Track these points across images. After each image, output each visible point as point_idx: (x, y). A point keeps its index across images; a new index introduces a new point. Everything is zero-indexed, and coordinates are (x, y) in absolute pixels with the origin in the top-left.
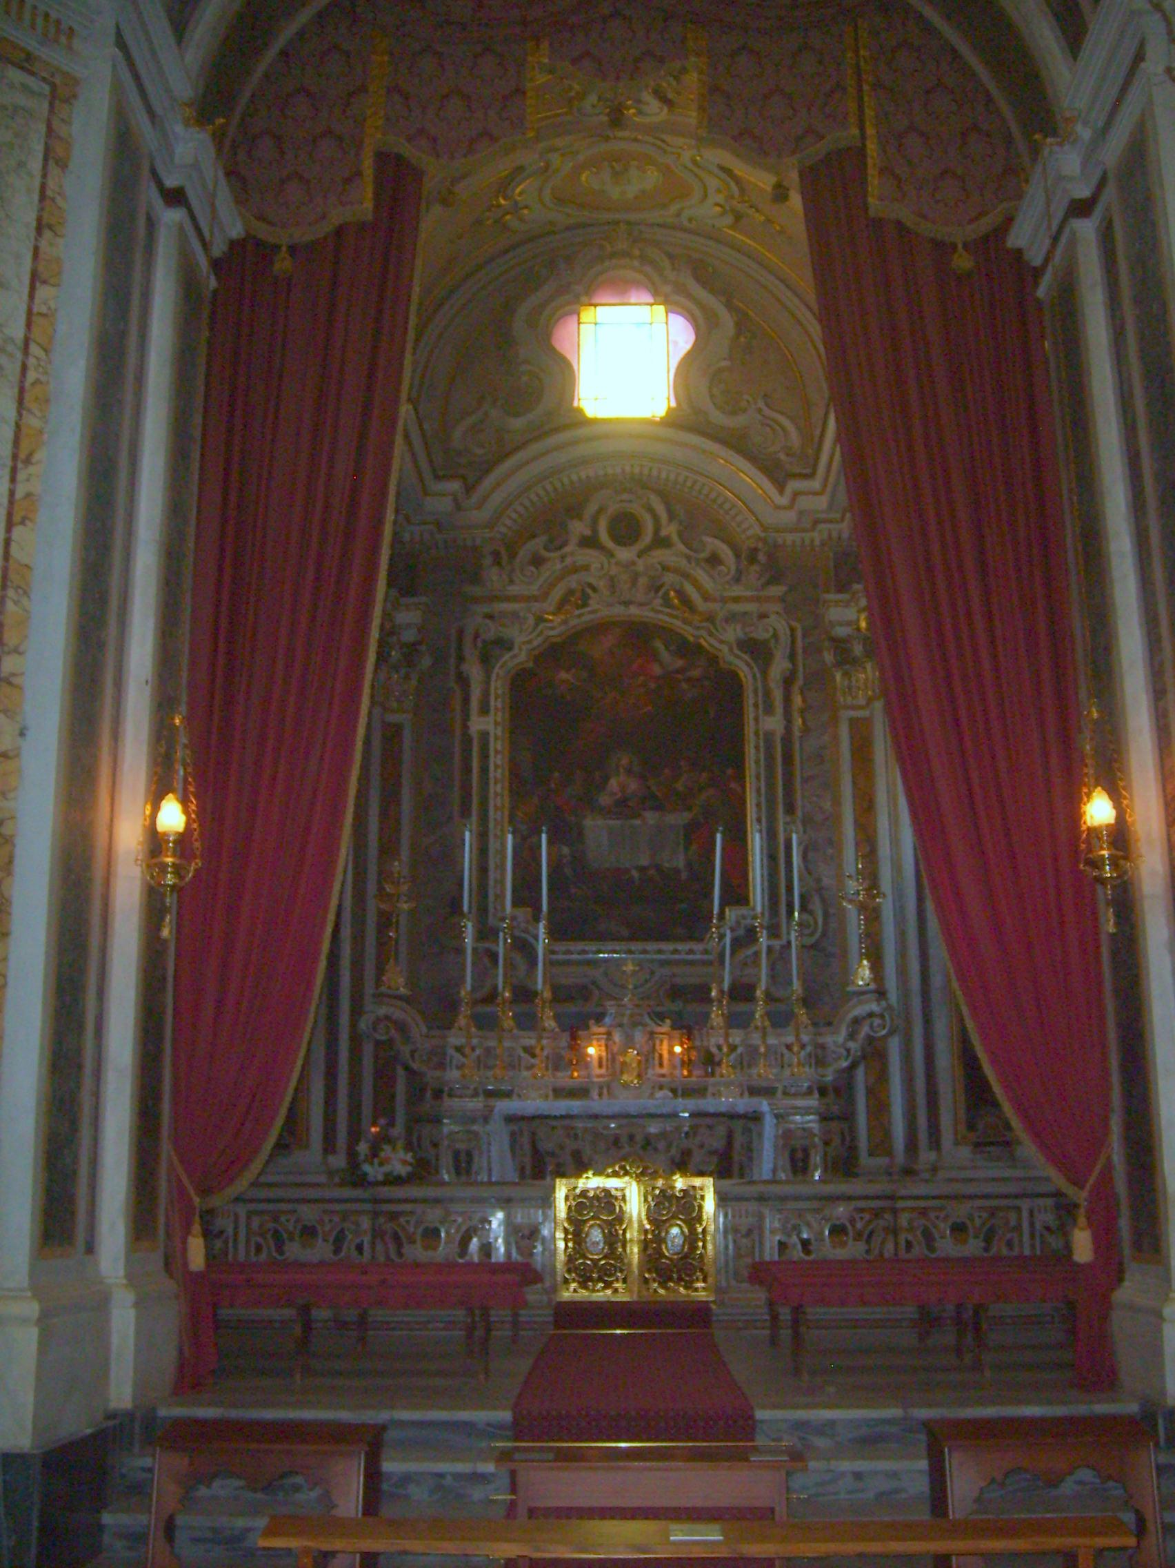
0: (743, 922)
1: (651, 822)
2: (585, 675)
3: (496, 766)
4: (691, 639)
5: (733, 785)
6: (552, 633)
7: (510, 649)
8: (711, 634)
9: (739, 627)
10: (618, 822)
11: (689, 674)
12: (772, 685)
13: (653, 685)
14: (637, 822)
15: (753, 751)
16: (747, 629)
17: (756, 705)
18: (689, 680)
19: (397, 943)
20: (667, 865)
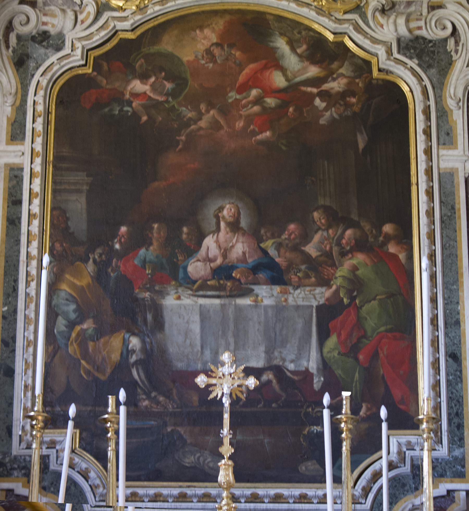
0: (409, 454)
1: (267, 302)
2: (169, 86)
3: (31, 216)
4: (330, 37)
5: (392, 249)
6: (120, 25)
7: (59, 48)
8: (358, 29)
9: (401, 21)
10: (217, 301)
11: (326, 86)
12: (451, 103)
13: (271, 102)
14: (246, 301)
15: (423, 197)
16: (413, 25)
17: (427, 132)
18: (324, 95)
19: (419, 435)
20: (291, 367)
